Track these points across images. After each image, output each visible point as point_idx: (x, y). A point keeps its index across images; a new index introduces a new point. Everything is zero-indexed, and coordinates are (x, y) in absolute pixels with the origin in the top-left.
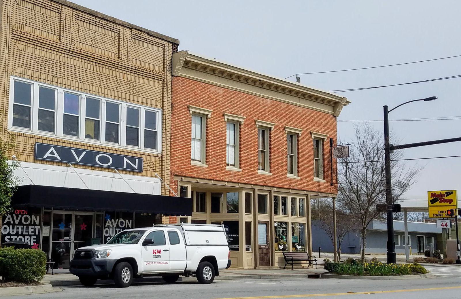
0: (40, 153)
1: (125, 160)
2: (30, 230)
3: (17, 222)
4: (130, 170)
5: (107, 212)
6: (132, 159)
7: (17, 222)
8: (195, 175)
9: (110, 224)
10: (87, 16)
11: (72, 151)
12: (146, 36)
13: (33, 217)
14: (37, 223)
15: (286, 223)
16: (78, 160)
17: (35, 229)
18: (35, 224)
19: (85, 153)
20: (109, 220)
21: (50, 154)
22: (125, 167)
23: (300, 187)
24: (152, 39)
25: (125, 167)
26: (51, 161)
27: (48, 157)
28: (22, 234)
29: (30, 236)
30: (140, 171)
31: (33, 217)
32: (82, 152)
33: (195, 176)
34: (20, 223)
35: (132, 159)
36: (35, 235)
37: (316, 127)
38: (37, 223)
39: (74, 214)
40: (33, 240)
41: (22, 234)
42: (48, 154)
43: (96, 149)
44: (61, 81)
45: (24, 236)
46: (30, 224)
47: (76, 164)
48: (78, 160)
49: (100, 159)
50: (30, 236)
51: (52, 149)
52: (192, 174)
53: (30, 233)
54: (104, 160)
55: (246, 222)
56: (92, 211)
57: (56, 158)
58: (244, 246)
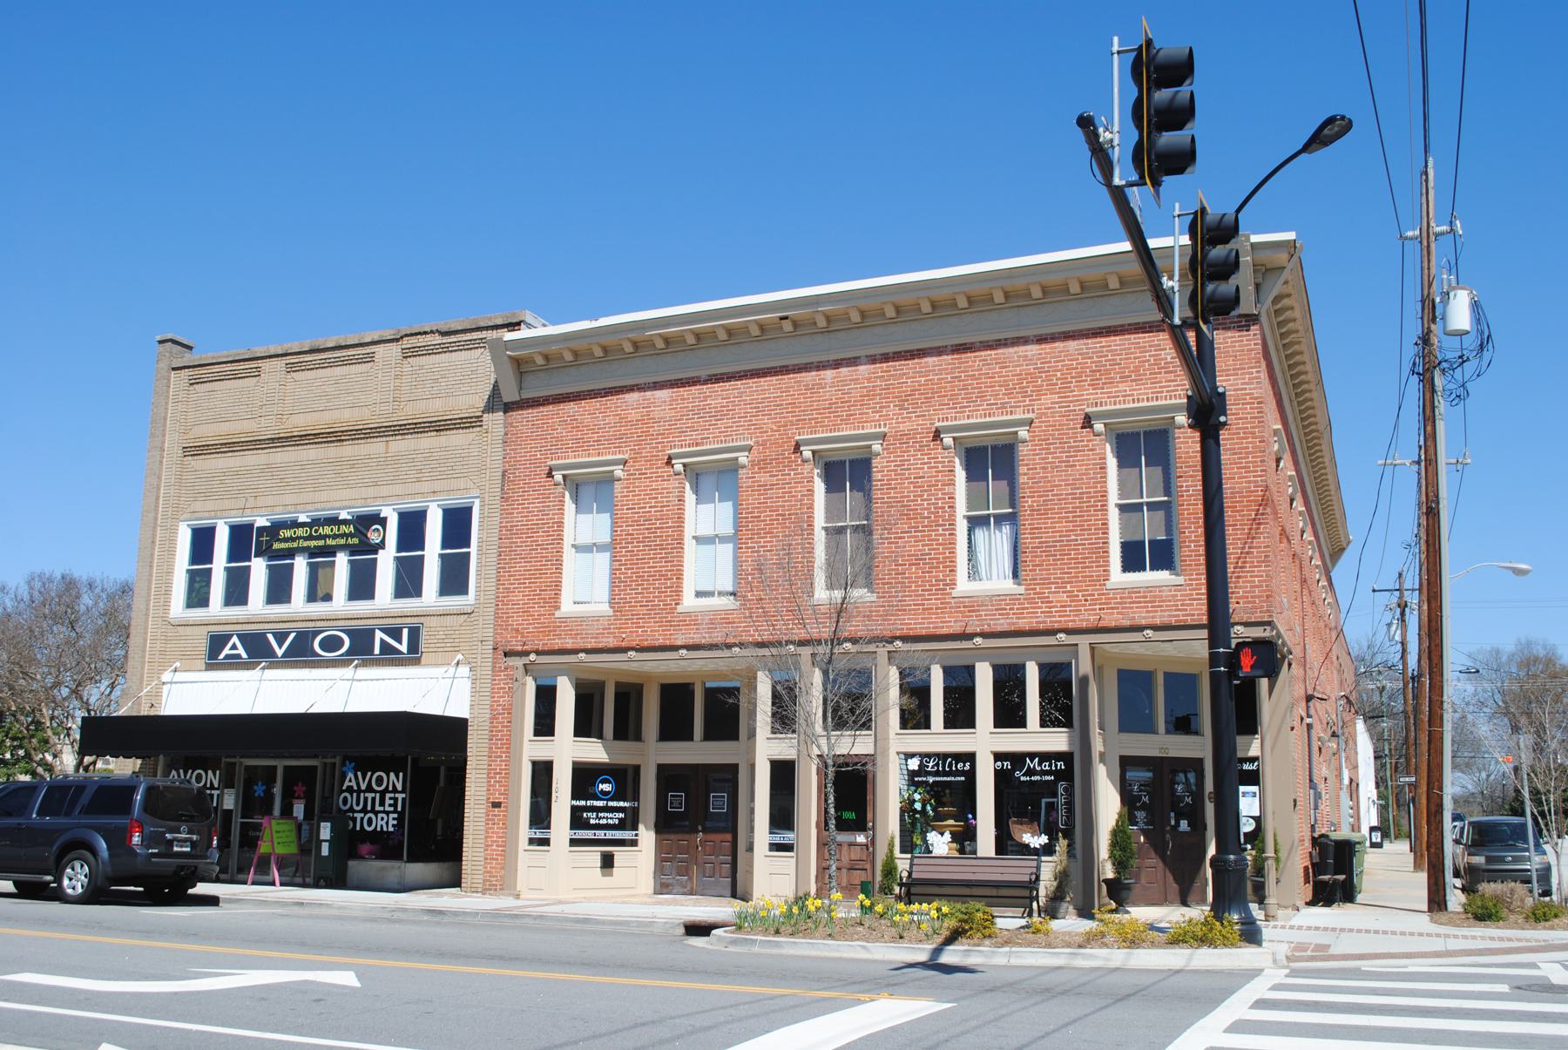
0: (215, 652)
1: (379, 635)
2: (388, 802)
3: (363, 787)
4: (390, 656)
5: (345, 759)
6: (395, 633)
7: (363, 787)
8: (569, 644)
9: (354, 784)
10: (309, 358)
11: (270, 637)
12: (437, 339)
13: (392, 775)
14: (399, 787)
15: (970, 757)
16: (280, 652)
17: (396, 800)
18: (395, 790)
19: (292, 636)
20: (351, 775)
21: (382, 641)
22: (377, 651)
23: (1024, 624)
24: (453, 338)
25: (377, 651)
26: (233, 663)
27: (227, 657)
28: (373, 811)
29: (388, 813)
30: (414, 655)
31: (392, 775)
32: (288, 634)
33: (569, 646)
34: (370, 789)
35: (395, 633)
36: (395, 811)
37: (1122, 387)
38: (399, 787)
39: (280, 764)
40: (392, 822)
41: (373, 811)
42: (227, 651)
43: (319, 624)
44: (261, 502)
45: (376, 813)
46: (386, 790)
47: (276, 664)
48: (280, 652)
49: (323, 645)
50: (388, 813)
51: (235, 639)
52: (557, 643)
53: (388, 808)
54: (331, 644)
55: (535, 764)
56: (316, 756)
57: (239, 656)
58: (762, 832)
